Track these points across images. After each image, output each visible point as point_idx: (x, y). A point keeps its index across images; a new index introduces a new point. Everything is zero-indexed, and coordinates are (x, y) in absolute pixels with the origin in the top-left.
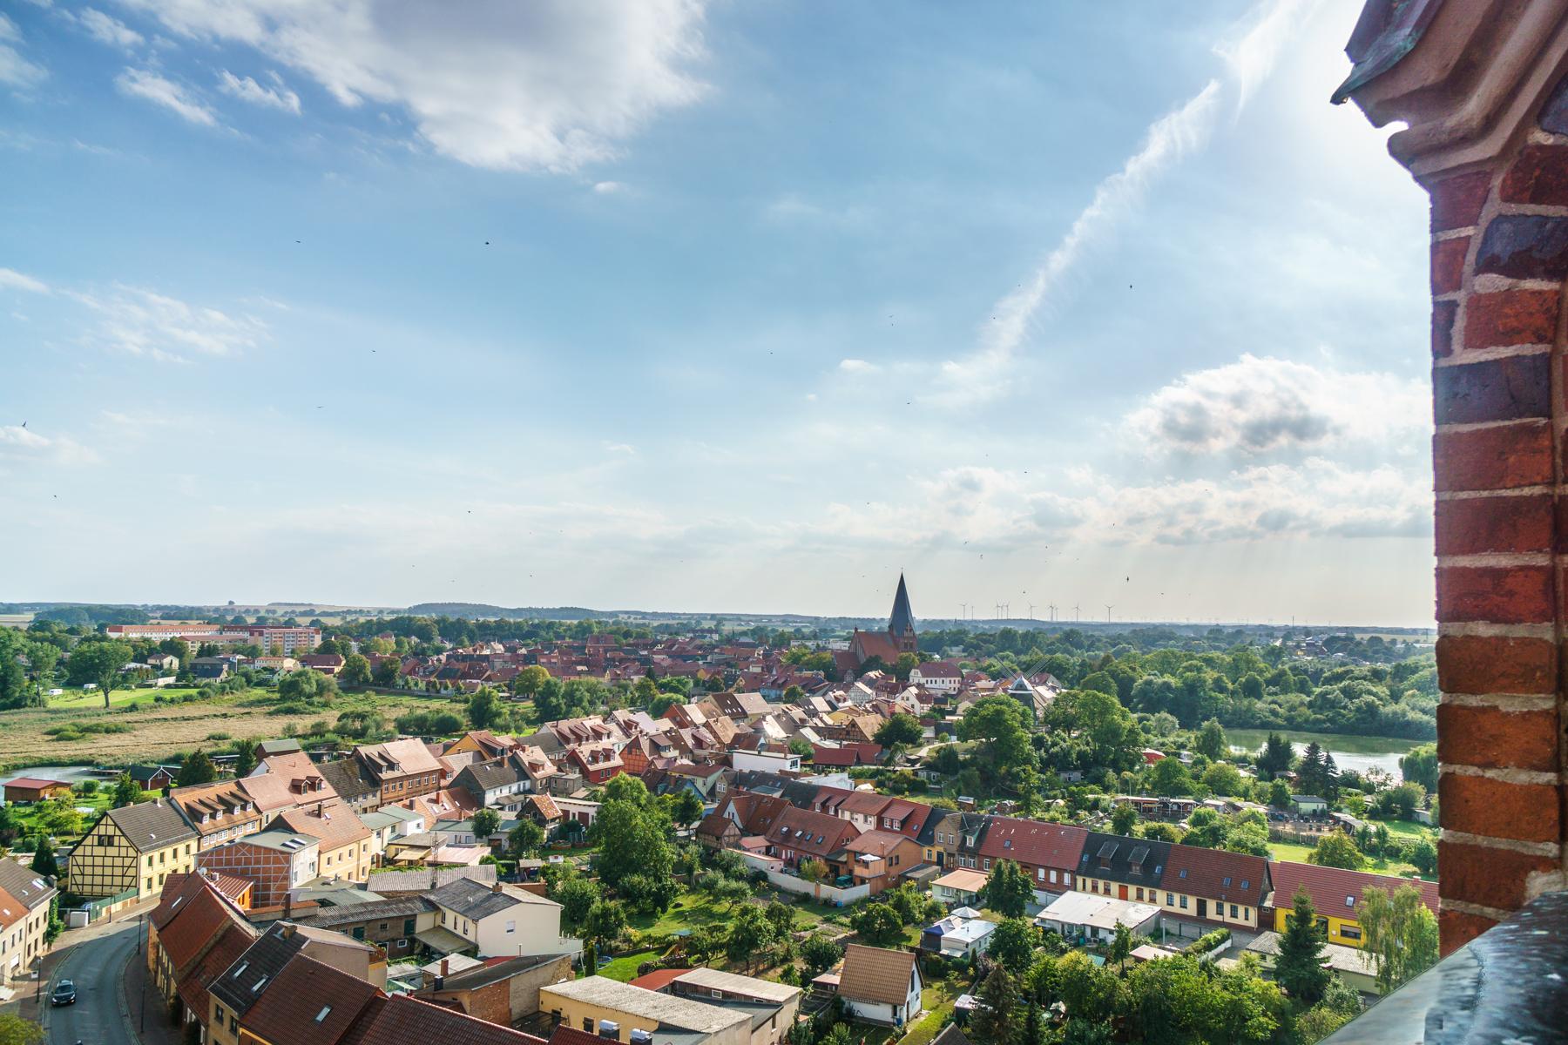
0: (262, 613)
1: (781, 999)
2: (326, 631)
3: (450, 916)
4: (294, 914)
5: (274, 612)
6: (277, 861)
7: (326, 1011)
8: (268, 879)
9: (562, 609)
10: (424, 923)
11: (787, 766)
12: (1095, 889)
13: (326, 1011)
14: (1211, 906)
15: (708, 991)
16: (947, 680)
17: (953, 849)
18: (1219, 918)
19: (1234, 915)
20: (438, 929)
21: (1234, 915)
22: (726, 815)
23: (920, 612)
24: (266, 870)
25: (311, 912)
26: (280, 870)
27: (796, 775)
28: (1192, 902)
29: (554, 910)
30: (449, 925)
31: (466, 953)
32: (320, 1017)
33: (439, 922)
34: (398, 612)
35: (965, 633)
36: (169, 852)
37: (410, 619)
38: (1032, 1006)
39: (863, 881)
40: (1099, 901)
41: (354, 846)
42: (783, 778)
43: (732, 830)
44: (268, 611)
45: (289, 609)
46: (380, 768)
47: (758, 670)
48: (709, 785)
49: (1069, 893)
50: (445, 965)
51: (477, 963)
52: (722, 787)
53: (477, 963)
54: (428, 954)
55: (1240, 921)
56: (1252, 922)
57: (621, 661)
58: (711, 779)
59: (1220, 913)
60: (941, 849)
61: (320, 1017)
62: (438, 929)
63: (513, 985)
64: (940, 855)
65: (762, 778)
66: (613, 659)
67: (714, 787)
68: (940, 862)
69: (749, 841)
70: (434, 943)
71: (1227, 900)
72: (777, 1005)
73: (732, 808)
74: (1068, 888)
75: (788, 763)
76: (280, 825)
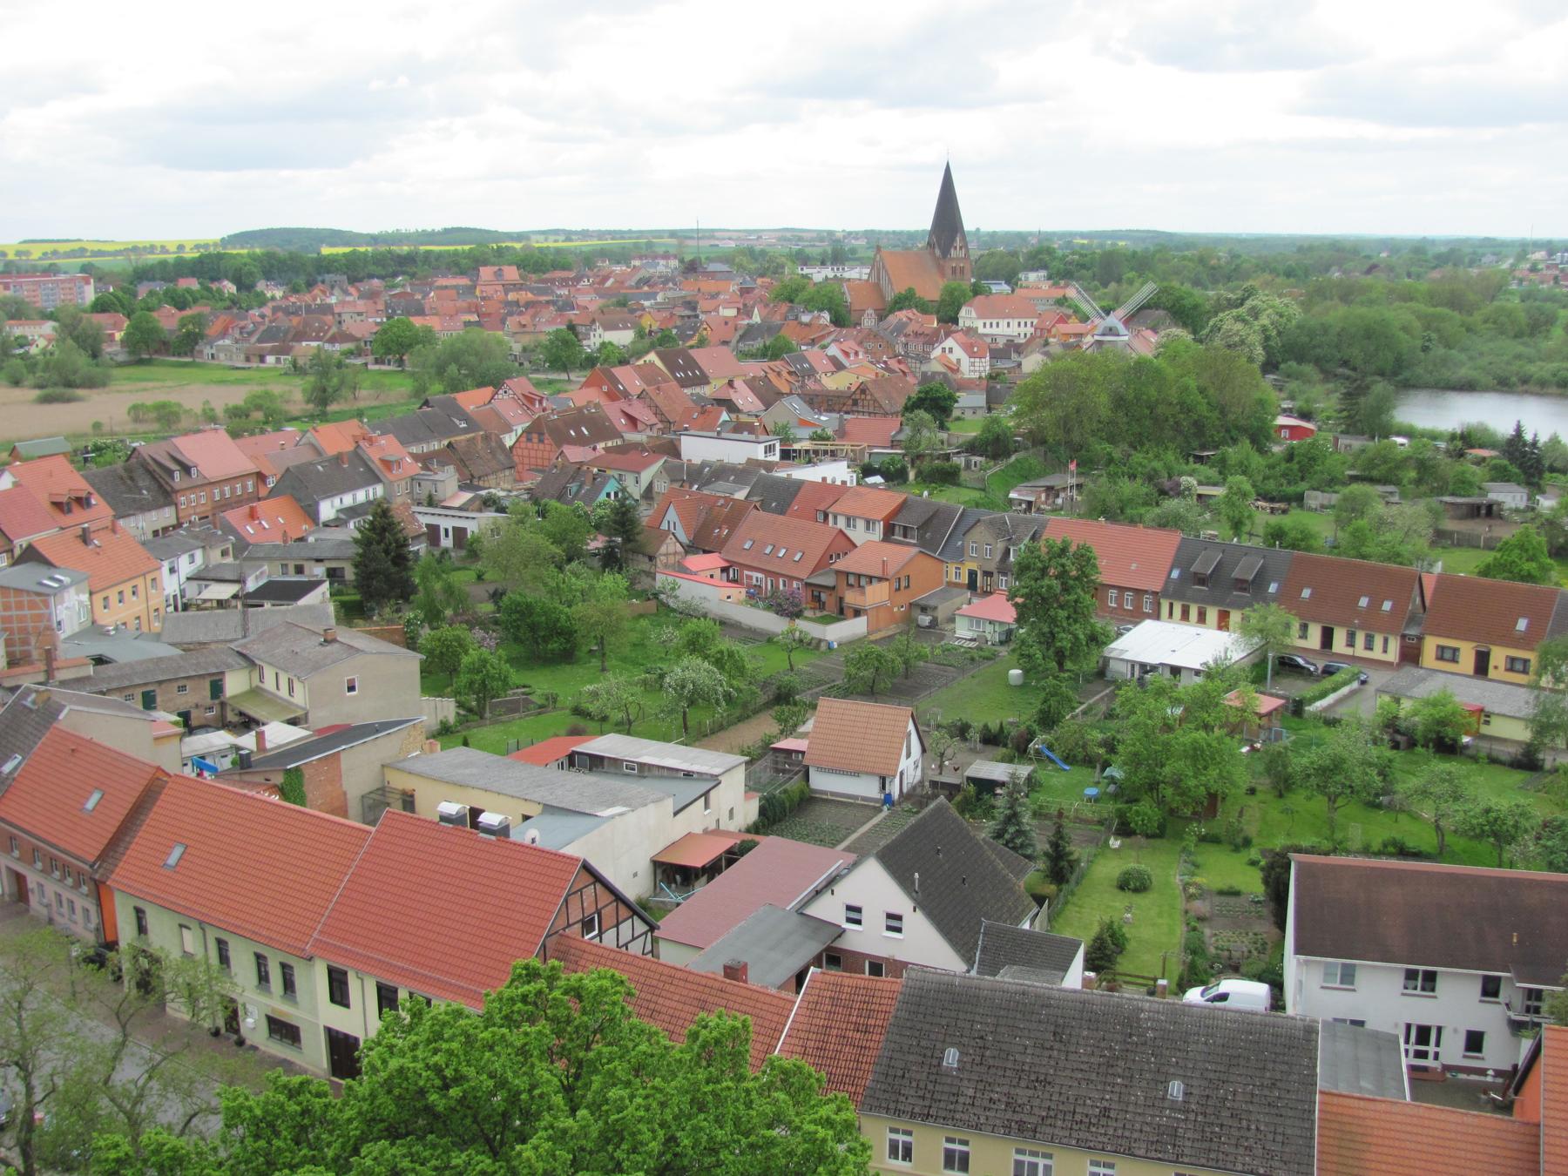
0: (11, 257)
1: (716, 771)
2: (101, 278)
3: (269, 674)
4: (62, 675)
5: (27, 253)
6: (33, 606)
7: (96, 797)
8: (23, 630)
9: (447, 231)
10: (235, 684)
11: (758, 452)
12: (1185, 616)
13: (96, 797)
14: (1339, 637)
15: (616, 762)
16: (1014, 323)
17: (992, 567)
18: (1349, 651)
19: (1369, 647)
20: (256, 692)
21: (1369, 647)
22: (664, 526)
23: (976, 217)
24: (21, 619)
25: (81, 673)
26: (39, 618)
27: (769, 466)
28: (1315, 632)
29: (411, 663)
30: (269, 684)
31: (293, 722)
32: (90, 805)
33: (256, 682)
34: (206, 246)
35: (1050, 251)
36: (113, 595)
37: (220, 257)
38: (137, 1152)
39: (857, 613)
40: (1190, 630)
41: (140, 582)
42: (740, 473)
43: (670, 547)
44: (18, 253)
45: (49, 248)
46: (170, 473)
47: (731, 312)
48: (644, 482)
49: (1148, 624)
50: (261, 737)
51: (305, 733)
52: (661, 487)
53: (305, 733)
54: (247, 723)
55: (1377, 654)
56: (1393, 655)
57: (529, 305)
58: (646, 476)
59: (1351, 644)
60: (974, 566)
61: (90, 805)
62: (256, 692)
63: (346, 762)
64: (972, 574)
65: (721, 472)
66: (517, 303)
67: (650, 486)
68: (972, 585)
69: (696, 561)
70: (253, 711)
71: (1361, 627)
72: (715, 780)
73: (672, 515)
74: (1149, 616)
75: (761, 447)
76: (31, 555)
